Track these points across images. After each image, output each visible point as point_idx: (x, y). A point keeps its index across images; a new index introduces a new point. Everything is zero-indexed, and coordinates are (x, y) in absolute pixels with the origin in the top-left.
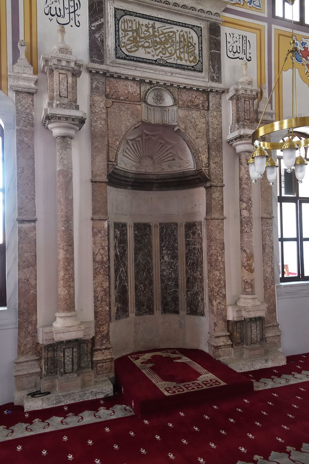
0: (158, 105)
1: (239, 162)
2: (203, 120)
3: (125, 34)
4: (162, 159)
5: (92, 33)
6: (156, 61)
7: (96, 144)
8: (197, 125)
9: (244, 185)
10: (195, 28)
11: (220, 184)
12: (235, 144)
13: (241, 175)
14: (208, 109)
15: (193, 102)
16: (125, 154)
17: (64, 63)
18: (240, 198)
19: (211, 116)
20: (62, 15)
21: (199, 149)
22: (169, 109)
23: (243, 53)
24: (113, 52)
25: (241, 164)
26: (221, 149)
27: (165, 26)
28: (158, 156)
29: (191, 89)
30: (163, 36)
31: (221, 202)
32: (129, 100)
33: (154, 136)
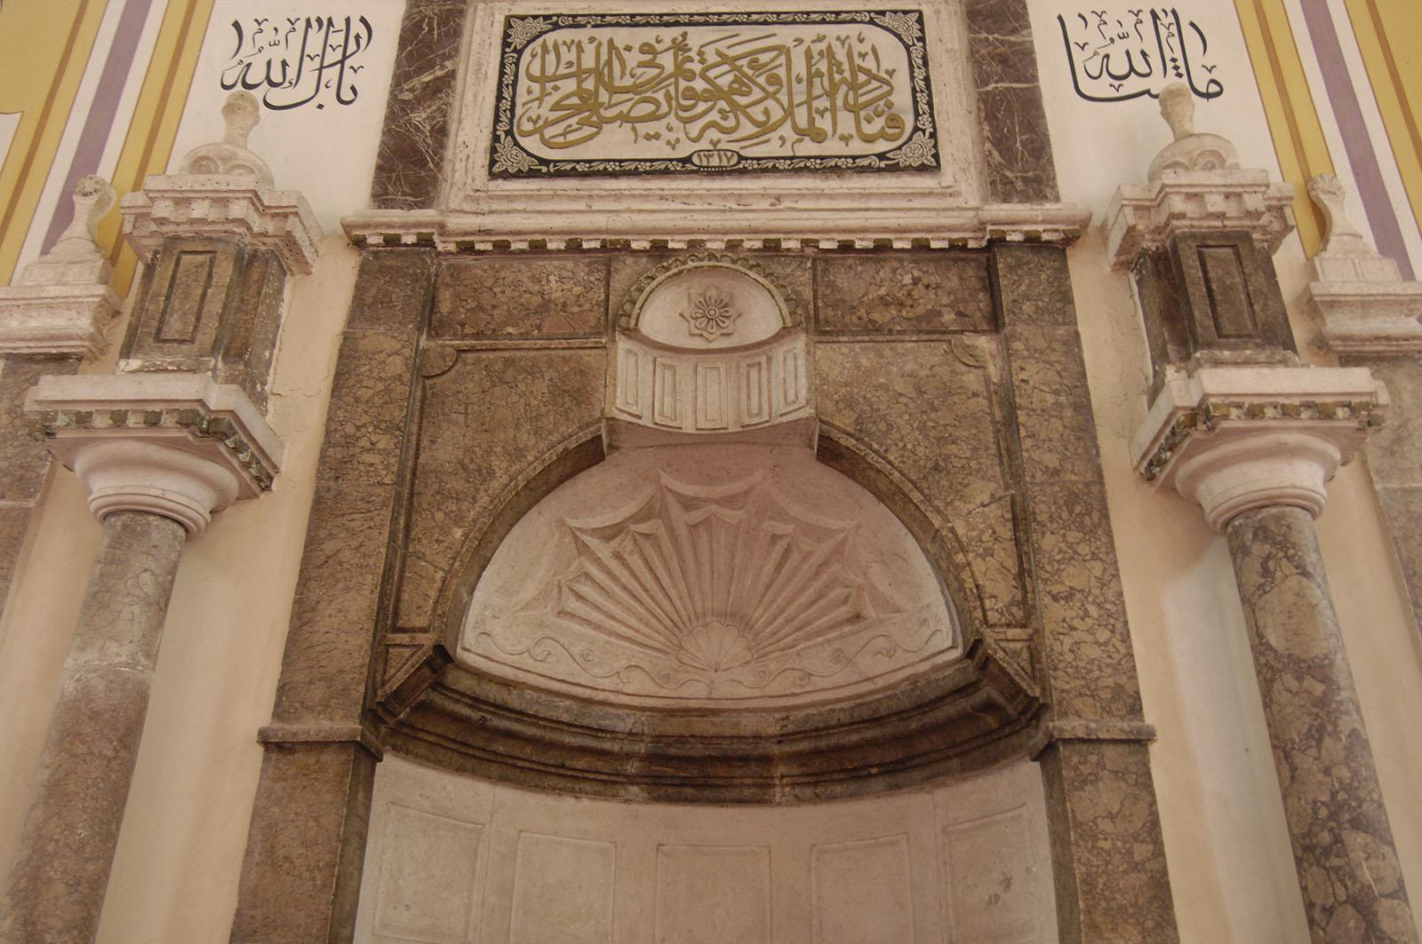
3: (543, 89)
4: (796, 623)
5: (397, 110)
6: (688, 160)
7: (329, 547)
10: (887, 20)
11: (1117, 726)
12: (1183, 471)
15: (901, 304)
16: (573, 605)
20: (288, 79)
23: (1171, 72)
26: (1096, 516)
29: (882, 248)
30: (726, 68)
31: (1142, 851)
33: (729, 501)
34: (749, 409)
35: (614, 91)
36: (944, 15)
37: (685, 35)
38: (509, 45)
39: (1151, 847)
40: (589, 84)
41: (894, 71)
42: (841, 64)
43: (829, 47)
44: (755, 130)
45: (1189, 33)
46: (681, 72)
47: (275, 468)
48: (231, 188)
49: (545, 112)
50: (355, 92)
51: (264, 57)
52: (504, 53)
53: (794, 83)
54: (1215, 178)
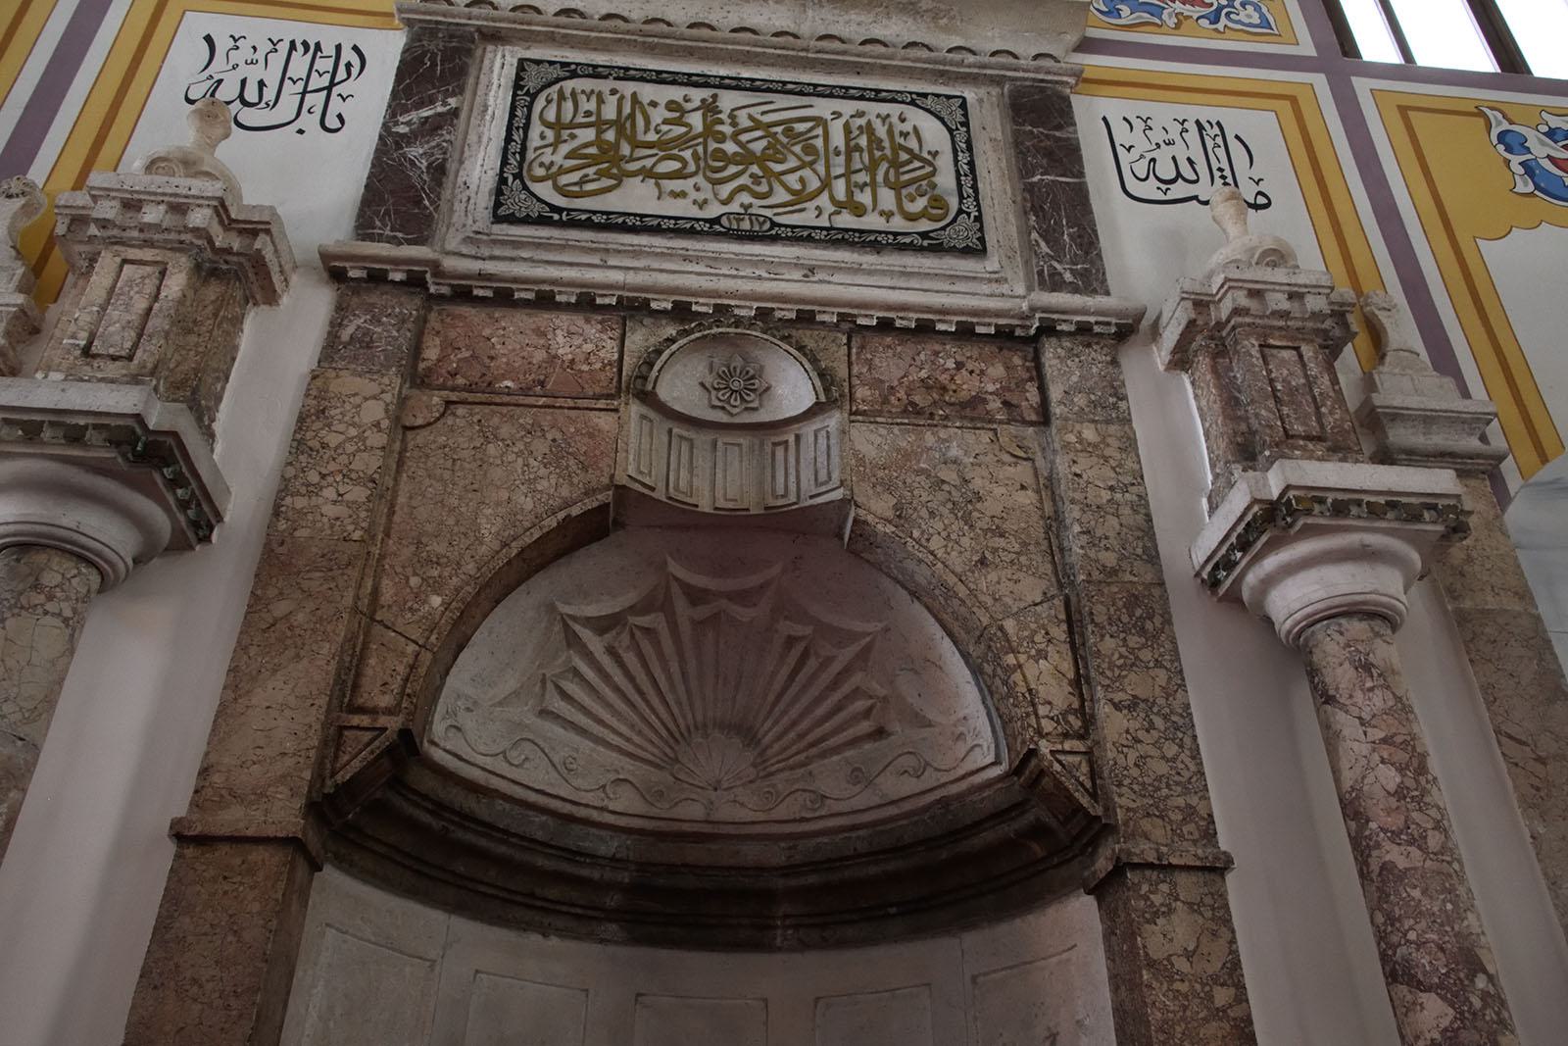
0: (737, 420)
1: (1314, 688)
2: (1023, 473)
4: (810, 738)
5: (389, 144)
6: (716, 221)
7: (281, 608)
8: (980, 499)
9: (1387, 845)
10: (929, 102)
12: (1251, 579)
13: (1348, 778)
14: (1044, 417)
15: (944, 389)
16: (558, 705)
17: (152, 215)
18: (1384, 958)
19: (1067, 446)
21: (1001, 628)
22: (803, 431)
23: (1218, 182)
24: (483, 201)
25: (1330, 700)
26: (1158, 620)
27: (771, 102)
28: (786, 720)
31: (1222, 996)
32: (547, 390)
33: (743, 597)
34: (774, 490)
35: (637, 146)
36: (986, 105)
37: (715, 97)
38: (522, 88)
39: (1232, 991)
40: (610, 135)
41: (937, 152)
42: (882, 141)
43: (869, 123)
44: (788, 197)
45: (1233, 144)
46: (709, 132)
47: (219, 518)
48: (193, 192)
49: (558, 159)
50: (342, 121)
51: (239, 74)
52: (515, 95)
53: (831, 155)
54: (1280, 275)
